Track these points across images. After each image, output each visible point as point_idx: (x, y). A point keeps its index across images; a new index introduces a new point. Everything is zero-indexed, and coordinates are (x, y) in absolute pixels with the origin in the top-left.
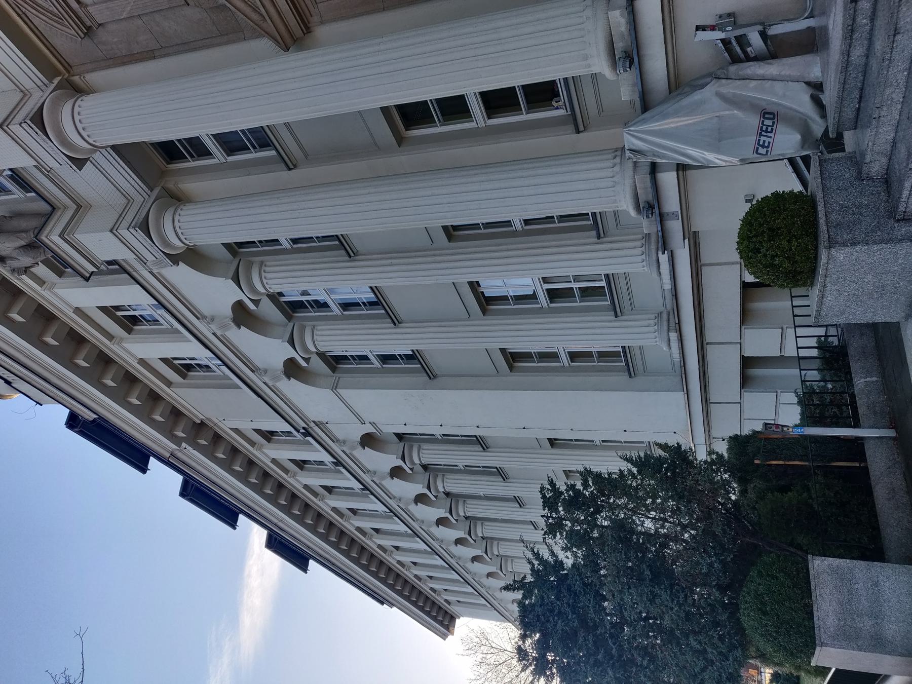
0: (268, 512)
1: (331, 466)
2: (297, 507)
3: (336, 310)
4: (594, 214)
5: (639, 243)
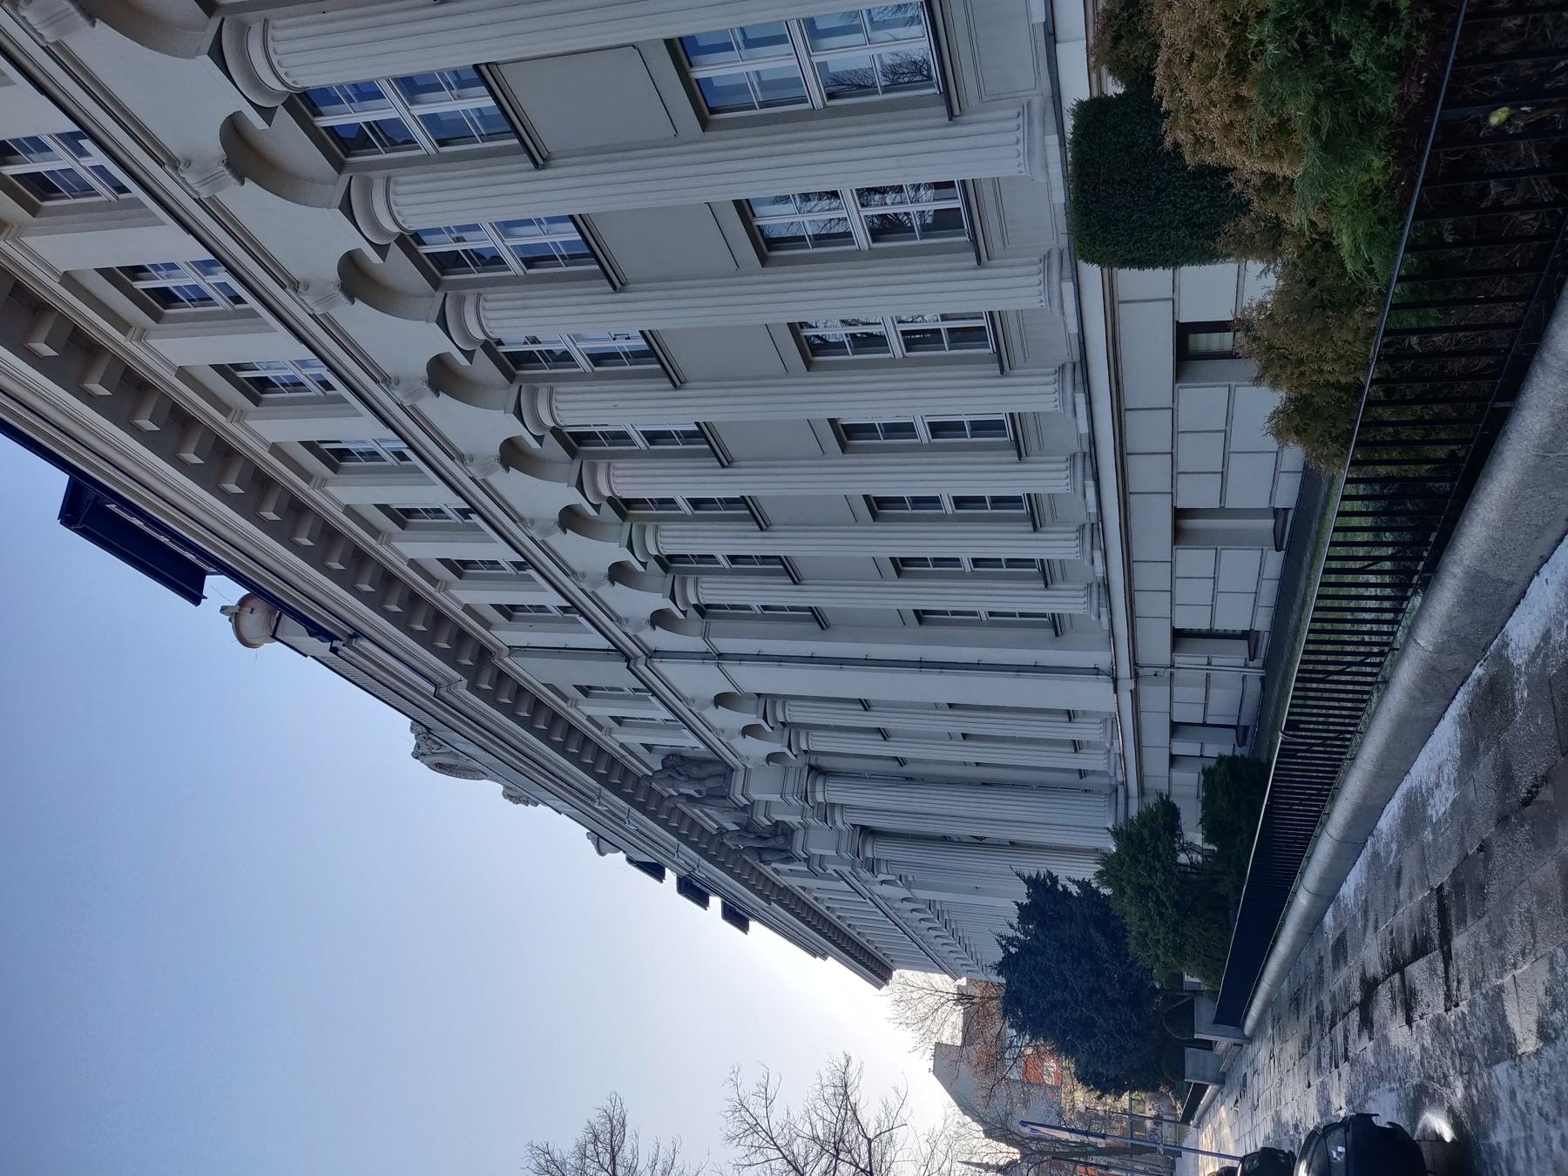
0: (489, 719)
3: (585, 365)
4: (991, 313)
5: (1073, 536)
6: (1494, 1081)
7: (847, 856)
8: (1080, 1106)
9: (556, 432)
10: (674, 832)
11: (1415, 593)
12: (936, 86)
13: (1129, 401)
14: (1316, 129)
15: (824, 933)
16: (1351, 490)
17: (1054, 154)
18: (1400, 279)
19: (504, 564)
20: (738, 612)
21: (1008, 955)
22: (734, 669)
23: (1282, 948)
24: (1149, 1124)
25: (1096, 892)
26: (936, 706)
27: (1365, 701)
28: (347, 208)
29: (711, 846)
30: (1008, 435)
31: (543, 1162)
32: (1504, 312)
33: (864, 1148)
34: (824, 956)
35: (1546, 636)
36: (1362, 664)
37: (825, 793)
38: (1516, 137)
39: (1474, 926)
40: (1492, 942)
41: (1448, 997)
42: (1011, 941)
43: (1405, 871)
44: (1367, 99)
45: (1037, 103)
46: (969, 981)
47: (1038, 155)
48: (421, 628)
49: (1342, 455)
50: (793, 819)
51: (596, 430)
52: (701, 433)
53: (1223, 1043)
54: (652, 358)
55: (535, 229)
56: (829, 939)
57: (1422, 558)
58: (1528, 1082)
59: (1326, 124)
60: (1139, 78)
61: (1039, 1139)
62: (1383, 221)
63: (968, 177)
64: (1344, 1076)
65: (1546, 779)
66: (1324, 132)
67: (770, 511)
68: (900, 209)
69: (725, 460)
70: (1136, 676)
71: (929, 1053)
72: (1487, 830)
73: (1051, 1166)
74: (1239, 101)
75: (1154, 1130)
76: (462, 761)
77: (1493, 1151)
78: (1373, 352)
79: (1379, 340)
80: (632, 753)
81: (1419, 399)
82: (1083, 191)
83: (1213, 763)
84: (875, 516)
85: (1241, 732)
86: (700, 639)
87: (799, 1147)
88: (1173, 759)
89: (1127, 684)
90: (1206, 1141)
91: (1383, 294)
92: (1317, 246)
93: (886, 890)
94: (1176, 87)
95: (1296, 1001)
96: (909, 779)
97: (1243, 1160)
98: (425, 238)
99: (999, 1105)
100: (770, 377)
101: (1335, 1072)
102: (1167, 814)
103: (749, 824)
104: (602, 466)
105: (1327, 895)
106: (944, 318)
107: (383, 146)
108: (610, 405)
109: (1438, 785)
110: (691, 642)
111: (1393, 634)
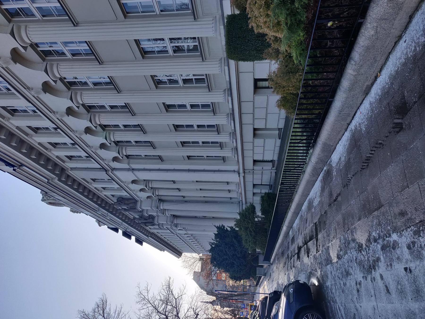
0: (65, 189)
1: (85, 158)
2: (70, 181)
3: (92, 86)
5: (222, 93)
6: (327, 270)
7: (169, 223)
8: (231, 285)
9: (83, 105)
10: (121, 219)
11: (311, 148)
12: (192, 11)
13: (242, 99)
14: (287, 24)
15: (163, 244)
16: (296, 121)
17: (222, 27)
18: (307, 65)
19: (68, 144)
20: (138, 157)
21: (212, 247)
22: (137, 173)
23: (280, 241)
24: (248, 287)
25: (235, 229)
26: (193, 182)
27: (299, 177)
28: (12, 34)
29: (131, 222)
30: (211, 108)
31: (82, 315)
32: (331, 76)
33: (174, 302)
34: (164, 250)
35: (340, 159)
36: (299, 167)
37: (163, 206)
38: (334, 29)
39: (323, 232)
40: (327, 235)
41: (317, 250)
42: (213, 244)
43: (308, 220)
44: (299, 16)
45: (218, 17)
46: (203, 255)
47: (218, 31)
48: (43, 163)
49: (294, 112)
50: (155, 214)
51: (95, 105)
52: (126, 106)
53: (265, 266)
54: (112, 84)
55: (75, 45)
56: (165, 246)
57: (312, 139)
58: (335, 269)
59: (289, 23)
60: (243, 9)
61: (221, 294)
62: (303, 50)
63: (200, 36)
64: (293, 271)
65: (339, 194)
66: (289, 25)
67: (146, 128)
68: (181, 44)
69: (133, 114)
70: (244, 172)
71: (192, 274)
72: (326, 208)
73: (223, 300)
74: (268, 15)
75: (249, 289)
76: (57, 201)
77: (327, 287)
78: (301, 85)
79: (302, 82)
80: (108, 197)
81: (312, 98)
82: (229, 39)
83: (263, 194)
84: (176, 130)
85: (270, 186)
86: (127, 165)
87: (156, 303)
88: (254, 194)
89: (242, 175)
90: (261, 291)
91: (303, 70)
92: (288, 57)
93: (180, 232)
94: (252, 11)
95: (283, 253)
96: (186, 202)
97: (269, 294)
98: (39, 45)
99: (211, 286)
100: (146, 90)
101: (291, 270)
102: (252, 208)
103: (142, 216)
104: (97, 115)
105: (290, 227)
106: (194, 75)
107: (24, 15)
108: (99, 97)
109: (316, 197)
110: (125, 166)
111: (306, 159)
